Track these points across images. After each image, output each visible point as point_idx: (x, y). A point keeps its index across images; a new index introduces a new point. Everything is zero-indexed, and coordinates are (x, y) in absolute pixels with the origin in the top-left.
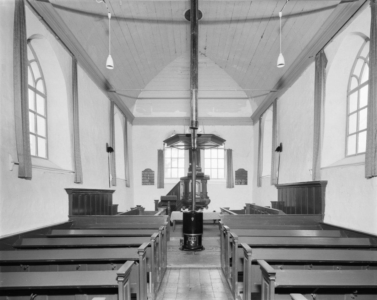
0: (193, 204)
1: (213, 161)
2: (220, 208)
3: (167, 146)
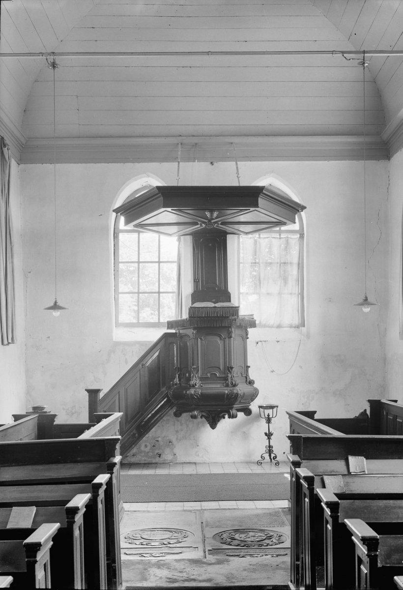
0: (265, 562)
1: (264, 275)
2: (288, 413)
3: (127, 222)
